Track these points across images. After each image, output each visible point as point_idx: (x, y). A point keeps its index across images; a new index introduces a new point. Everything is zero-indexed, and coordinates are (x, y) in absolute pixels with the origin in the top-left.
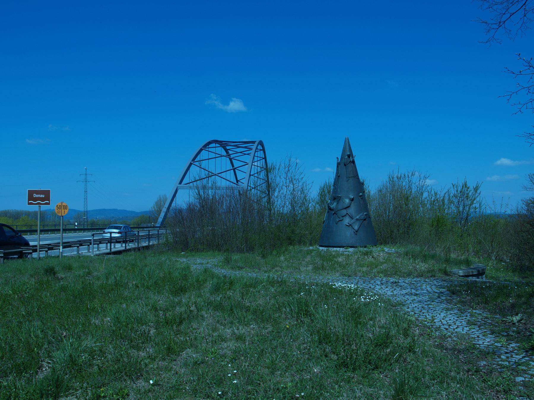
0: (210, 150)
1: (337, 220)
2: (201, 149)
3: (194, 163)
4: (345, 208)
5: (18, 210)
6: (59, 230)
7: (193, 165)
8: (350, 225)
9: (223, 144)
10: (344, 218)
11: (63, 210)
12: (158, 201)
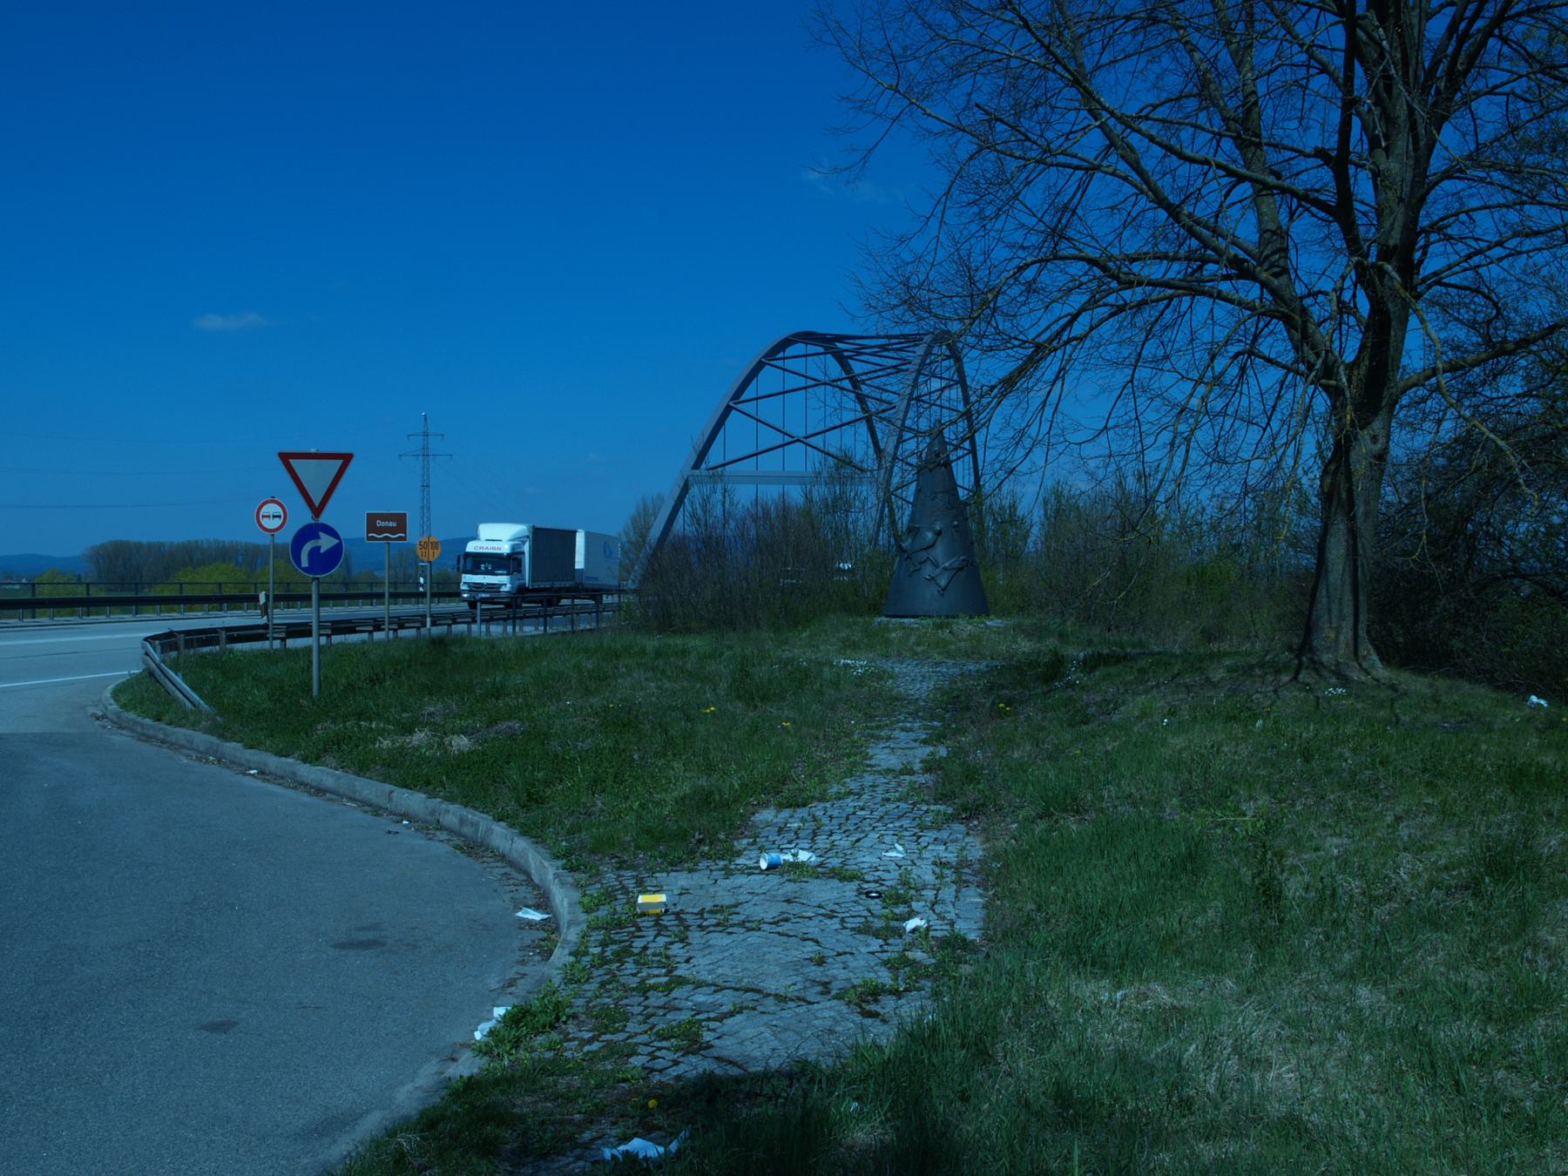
0: (789, 364)
1: (911, 570)
2: (760, 362)
3: (738, 406)
4: (925, 549)
5: (224, 542)
6: (381, 596)
7: (734, 411)
8: (933, 578)
9: (827, 342)
10: (923, 566)
11: (431, 551)
12: (639, 514)
